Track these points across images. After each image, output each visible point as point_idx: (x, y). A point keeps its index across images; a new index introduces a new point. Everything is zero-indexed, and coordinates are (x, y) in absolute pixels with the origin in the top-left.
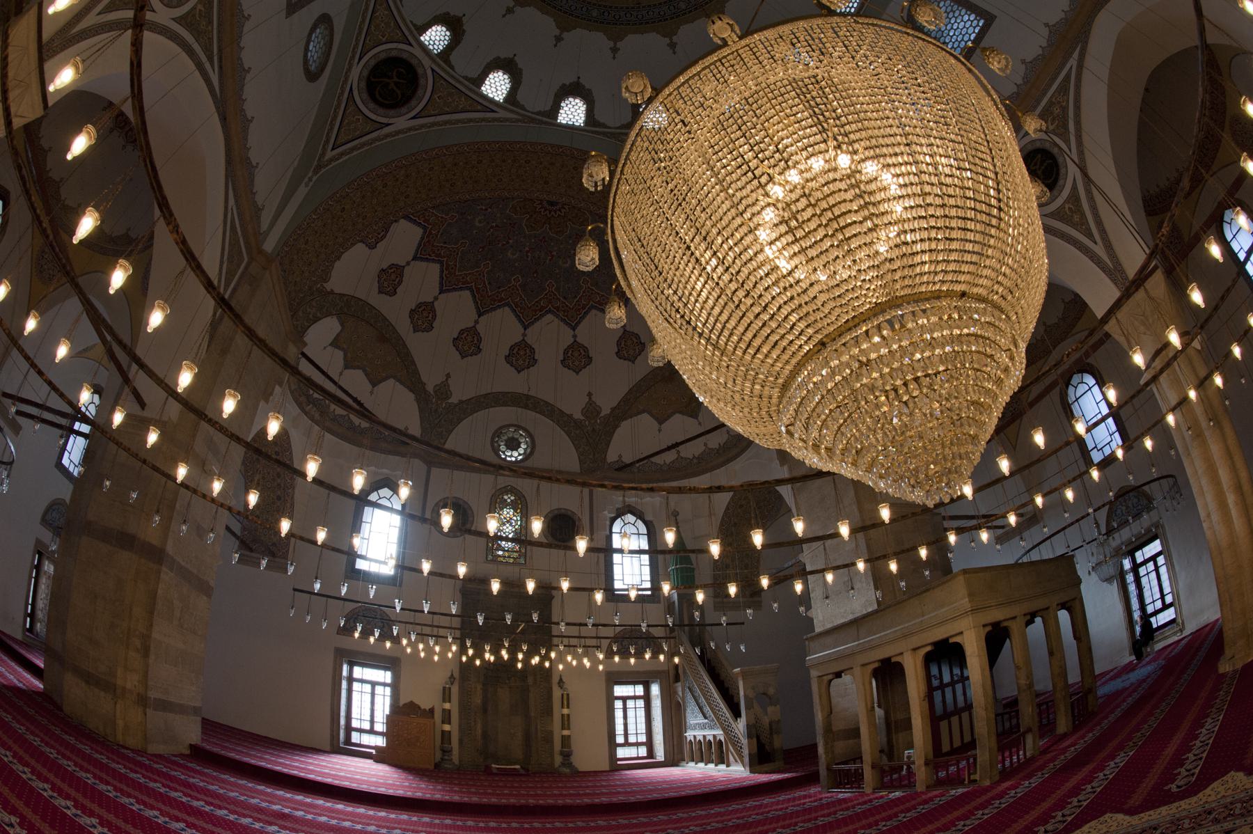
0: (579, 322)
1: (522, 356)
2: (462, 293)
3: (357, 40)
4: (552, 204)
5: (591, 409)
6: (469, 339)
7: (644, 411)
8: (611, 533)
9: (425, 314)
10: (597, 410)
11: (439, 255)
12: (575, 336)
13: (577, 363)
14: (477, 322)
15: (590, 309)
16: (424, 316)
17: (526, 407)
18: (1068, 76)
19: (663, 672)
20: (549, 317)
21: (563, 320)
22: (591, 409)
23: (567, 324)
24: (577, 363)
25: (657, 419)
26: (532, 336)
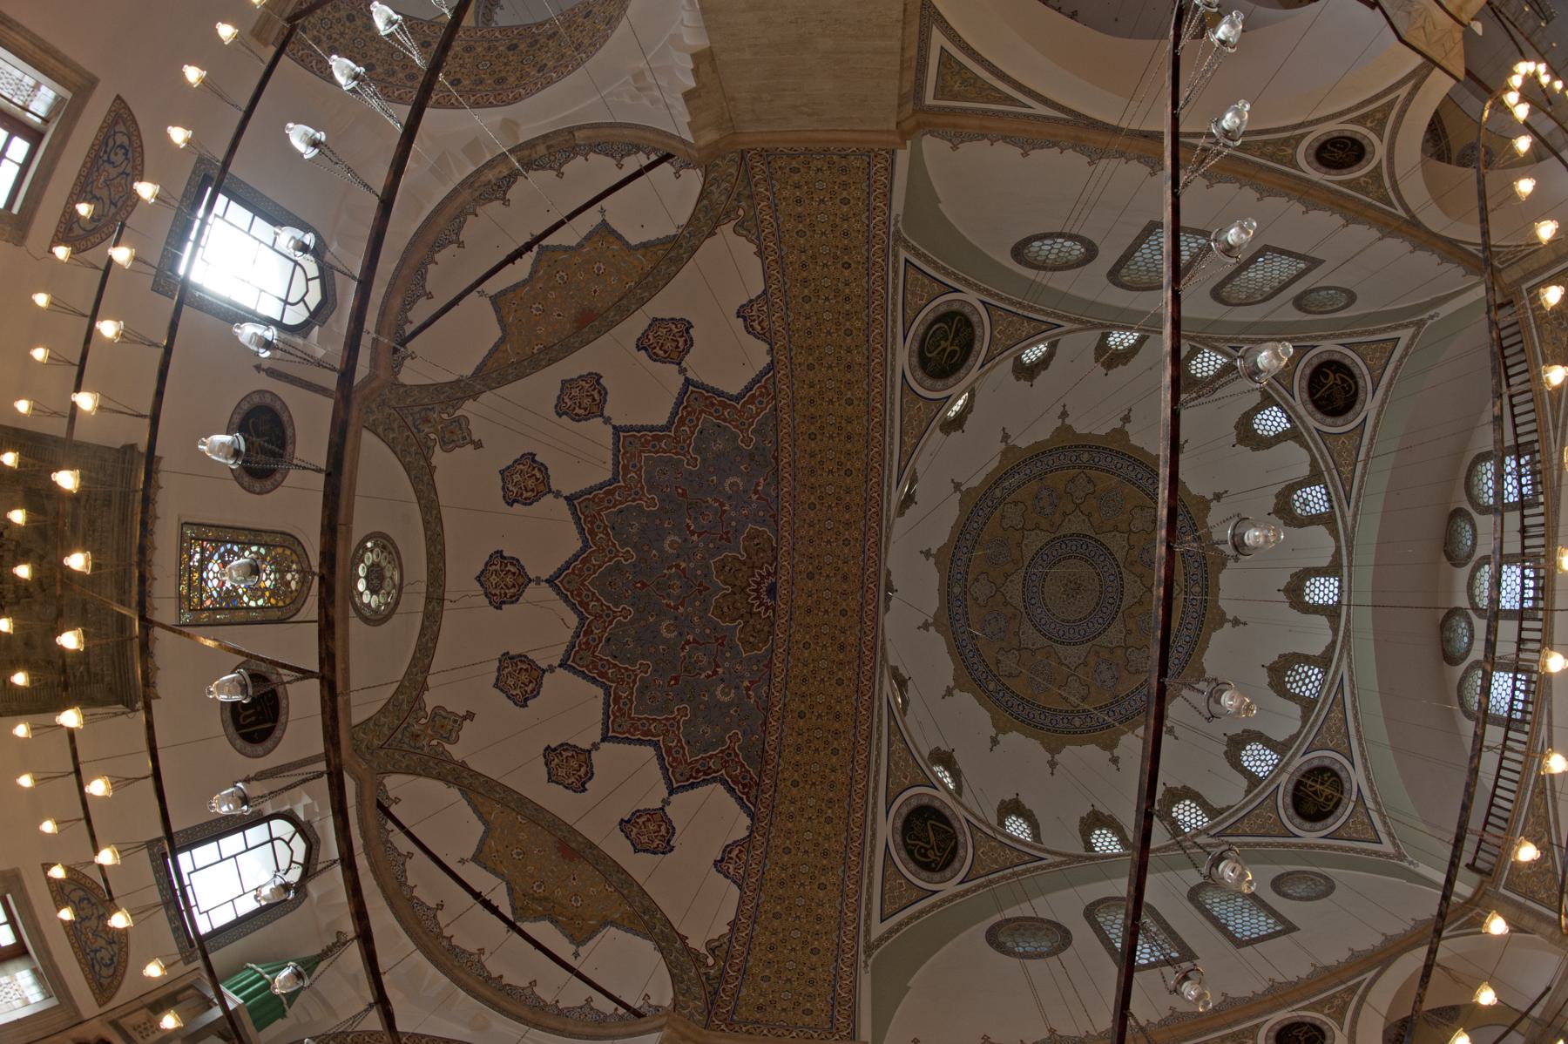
0: (575, 672)
1: (504, 580)
2: (610, 466)
3: (1001, 299)
4: (772, 591)
5: (448, 724)
6: (531, 483)
7: (485, 822)
8: (267, 819)
10: (451, 737)
12: (551, 669)
13: (511, 681)
14: (557, 494)
15: (602, 685)
16: (584, 400)
17: (429, 599)
18: (1359, 984)
19: (77, 1011)
20: (573, 620)
22: (448, 724)
24: (511, 681)
25: (479, 850)
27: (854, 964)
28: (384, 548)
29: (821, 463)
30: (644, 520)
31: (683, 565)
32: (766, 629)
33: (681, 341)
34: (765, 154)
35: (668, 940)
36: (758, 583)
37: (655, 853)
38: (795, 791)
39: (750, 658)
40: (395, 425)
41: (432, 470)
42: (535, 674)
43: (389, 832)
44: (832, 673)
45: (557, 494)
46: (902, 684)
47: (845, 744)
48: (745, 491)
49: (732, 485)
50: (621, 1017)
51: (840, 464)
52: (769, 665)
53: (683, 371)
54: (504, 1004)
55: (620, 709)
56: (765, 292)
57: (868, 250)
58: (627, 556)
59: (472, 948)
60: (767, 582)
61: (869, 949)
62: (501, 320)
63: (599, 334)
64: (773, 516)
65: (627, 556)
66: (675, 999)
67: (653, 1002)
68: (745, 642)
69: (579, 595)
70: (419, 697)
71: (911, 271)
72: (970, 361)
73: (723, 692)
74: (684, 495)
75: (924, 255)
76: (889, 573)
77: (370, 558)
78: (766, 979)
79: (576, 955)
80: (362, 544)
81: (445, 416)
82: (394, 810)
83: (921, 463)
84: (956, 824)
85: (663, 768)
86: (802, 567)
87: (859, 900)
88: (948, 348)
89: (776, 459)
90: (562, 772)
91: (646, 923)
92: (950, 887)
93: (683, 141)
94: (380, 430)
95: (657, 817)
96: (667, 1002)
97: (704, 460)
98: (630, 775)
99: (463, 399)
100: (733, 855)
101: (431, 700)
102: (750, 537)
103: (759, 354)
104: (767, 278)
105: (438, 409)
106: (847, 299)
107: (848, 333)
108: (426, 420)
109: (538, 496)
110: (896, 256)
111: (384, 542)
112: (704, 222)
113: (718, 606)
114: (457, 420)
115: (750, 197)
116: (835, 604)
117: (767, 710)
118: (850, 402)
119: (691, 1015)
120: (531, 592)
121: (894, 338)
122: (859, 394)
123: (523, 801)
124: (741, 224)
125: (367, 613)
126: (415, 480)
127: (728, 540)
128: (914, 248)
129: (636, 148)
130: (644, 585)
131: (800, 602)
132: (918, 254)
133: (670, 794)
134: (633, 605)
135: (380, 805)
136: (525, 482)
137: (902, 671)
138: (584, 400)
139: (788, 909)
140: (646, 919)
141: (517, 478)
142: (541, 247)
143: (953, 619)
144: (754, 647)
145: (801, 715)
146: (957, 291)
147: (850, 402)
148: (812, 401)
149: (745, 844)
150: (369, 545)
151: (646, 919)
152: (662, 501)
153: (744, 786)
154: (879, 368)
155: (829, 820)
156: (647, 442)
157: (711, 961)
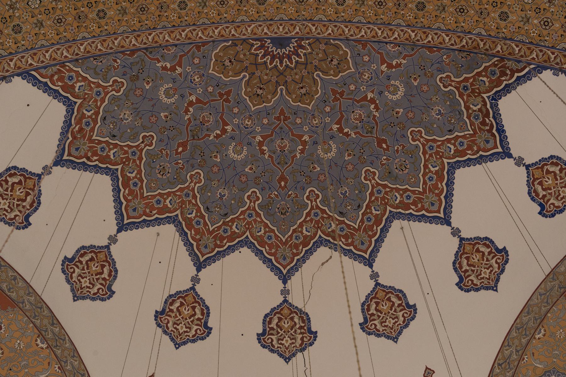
4: (281, 42)
12: (375, 276)
13: (390, 322)
14: (195, 280)
15: (389, 221)
16: (92, 271)
20: (323, 252)
21: (347, 253)
23: (356, 257)
30: (215, 183)
32: (322, 46)
36: (273, 58)
39: (356, 64)
45: (195, 280)
48: (174, 81)
49: (168, 95)
52: (364, 43)
55: (415, 203)
58: (253, 198)
60: (272, 49)
65: (253, 198)
68: (338, 69)
69: (296, 246)
73: (394, 93)
74: (184, 145)
89: (133, 52)
97: (145, 129)
102: (224, 70)
109: (199, 301)
113: (300, 98)
117: (414, 45)
120: (296, 300)
123: (518, 326)
127: (228, 93)
130: (282, 178)
134: (304, 189)
138: (92, 271)
141: (182, 328)
144: (343, 59)
148: (59, 21)
153: (503, 74)
156: (131, 192)
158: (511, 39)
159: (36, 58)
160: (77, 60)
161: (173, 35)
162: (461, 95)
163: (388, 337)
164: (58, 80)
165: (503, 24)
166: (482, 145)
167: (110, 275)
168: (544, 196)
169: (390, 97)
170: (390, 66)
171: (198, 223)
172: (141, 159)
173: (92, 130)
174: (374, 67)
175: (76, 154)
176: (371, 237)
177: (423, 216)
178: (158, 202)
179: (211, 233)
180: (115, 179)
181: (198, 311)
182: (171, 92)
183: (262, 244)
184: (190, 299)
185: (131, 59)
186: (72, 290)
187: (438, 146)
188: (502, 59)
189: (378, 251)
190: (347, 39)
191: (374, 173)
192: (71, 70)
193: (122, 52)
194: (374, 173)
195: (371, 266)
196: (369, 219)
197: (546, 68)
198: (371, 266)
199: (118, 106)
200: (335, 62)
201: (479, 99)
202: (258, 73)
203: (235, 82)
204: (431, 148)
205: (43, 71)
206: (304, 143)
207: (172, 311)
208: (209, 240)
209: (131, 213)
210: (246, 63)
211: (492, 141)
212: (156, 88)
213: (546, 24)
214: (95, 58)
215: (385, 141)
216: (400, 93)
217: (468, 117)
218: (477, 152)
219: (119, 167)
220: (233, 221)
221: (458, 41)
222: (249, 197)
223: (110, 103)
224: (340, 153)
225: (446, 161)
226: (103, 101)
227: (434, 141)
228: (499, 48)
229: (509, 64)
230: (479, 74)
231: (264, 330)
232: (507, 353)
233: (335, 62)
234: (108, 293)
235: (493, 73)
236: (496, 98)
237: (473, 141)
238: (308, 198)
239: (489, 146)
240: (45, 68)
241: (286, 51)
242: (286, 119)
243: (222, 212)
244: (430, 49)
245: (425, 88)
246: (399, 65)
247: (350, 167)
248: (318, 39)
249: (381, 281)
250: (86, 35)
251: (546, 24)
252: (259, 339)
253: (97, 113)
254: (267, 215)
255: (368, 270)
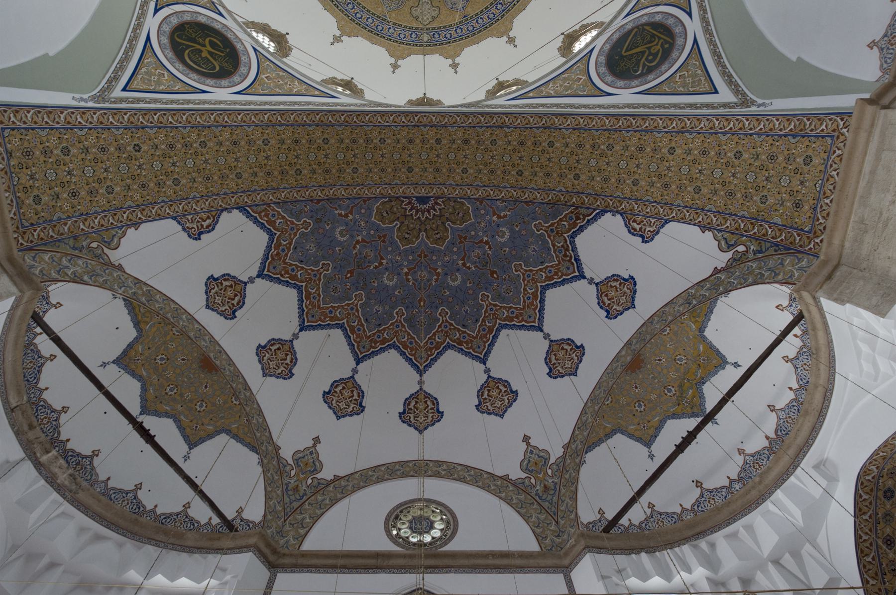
4: (423, 200)
5: (535, 460)
6: (347, 394)
9: (280, 355)
10: (544, 456)
11: (293, 277)
12: (487, 371)
13: (498, 404)
14: (355, 371)
20: (450, 353)
22: (535, 460)
25: (639, 440)
26: (433, 381)
27: (758, 117)
28: (397, 517)
29: (319, 164)
30: (373, 302)
31: (406, 270)
32: (452, 204)
33: (225, 283)
34: (22, 229)
35: (718, 284)
37: (635, 292)
38: (583, 177)
39: (475, 216)
40: (299, 517)
41: (337, 478)
42: (492, 384)
43: (631, 524)
44: (486, 150)
45: (355, 371)
46: (501, 86)
47: (545, 136)
50: (805, 332)
51: (319, 148)
52: (480, 200)
53: (251, 280)
54: (800, 440)
55: (517, 317)
56: (174, 218)
57: (118, 128)
59: (740, 460)
60: (417, 205)
61: (745, 102)
62: (210, 436)
63: (222, 351)
64: (365, 201)
66: (781, 283)
67: (785, 303)
68: (463, 220)
70: (514, 483)
71: (134, 85)
72: (217, 26)
74: (351, 272)
75: (116, 71)
76: (410, 102)
77: (405, 532)
78: (764, 199)
79: (736, 365)
80: (394, 539)
81: (293, 473)
82: (610, 516)
83: (316, 73)
84: (629, 27)
85: (563, 282)
86: (404, 177)
87: (689, 117)
88: (206, 48)
89: (319, 201)
90: (568, 364)
91: (700, 303)
92: (693, 26)
93: (14, 308)
94: (302, 532)
95: (604, 288)
96: (786, 290)
97: (324, 258)
98: (569, 309)
99: (279, 458)
100: (638, 227)
101: (516, 473)
103: (233, 222)
104: (160, 217)
105: (286, 480)
106: (171, 146)
107: (203, 145)
108: (296, 489)
110: (121, 100)
111: (393, 518)
112: (108, 276)
113: (436, 241)
114: (296, 461)
115: (75, 238)
116: (431, 148)
117: (516, 201)
118: (266, 142)
119: (801, 269)
121: (205, 102)
122: (258, 134)
124: (108, 244)
125: (449, 533)
126: (345, 493)
127: (385, 236)
128: (109, 81)
129: (30, 348)
131: (431, 177)
132: (115, 78)
133: (584, 277)
134: (437, 308)
135: (607, 530)
136: (345, 398)
137: (490, 86)
139: (691, 180)
140: (699, 301)
141: (342, 405)
142: (144, 410)
143: (447, 39)
144: (466, 213)
145: (520, 173)
146: (148, 38)
147: (266, 142)
149: (628, 218)
150: (395, 532)
151: (699, 301)
152: (357, 289)
153: (578, 218)
154: (233, 116)
155: (610, 147)
157: (741, 248)
158: (582, 193)
159: (250, 198)
160: (279, 203)
161: (347, 191)
162: (549, 237)
163: (496, 415)
164: (265, 216)
165: (576, 182)
166: (564, 271)
167: (291, 362)
168: (609, 304)
169: (499, 239)
170: (499, 217)
171: (359, 330)
172: (320, 280)
173: (286, 255)
174: (488, 218)
175: (273, 271)
176: (485, 342)
177: (523, 325)
178: (331, 312)
179: (368, 337)
180: (300, 292)
181: (355, 394)
182: (344, 233)
183: (406, 347)
184: (350, 384)
185: (317, 206)
186: (263, 369)
187: (534, 275)
188: (577, 208)
189: (490, 352)
190: (469, 198)
191: (488, 296)
192: (273, 210)
193: (311, 201)
194: (488, 296)
195: (485, 364)
196: (484, 330)
197: (607, 212)
198: (485, 364)
199: (306, 240)
200: (461, 215)
201: (562, 238)
202: (406, 222)
203: (391, 228)
204: (529, 276)
205: (254, 208)
206: (438, 274)
207: (336, 392)
208: (366, 342)
209: (310, 319)
210: (398, 215)
211: (571, 268)
212: (333, 229)
213: (606, 180)
214: (292, 202)
215: (495, 272)
216: (507, 237)
217: (555, 252)
218: (561, 276)
219: (304, 284)
220: (384, 330)
221: (546, 196)
222: (397, 313)
223: (300, 237)
224: (464, 282)
225: (539, 285)
226: (295, 235)
227: (531, 271)
228: (574, 200)
229: (582, 210)
230: (561, 220)
231: (404, 410)
232: (584, 419)
233: (461, 215)
234: (289, 375)
235: (571, 219)
236: (573, 237)
237: (558, 269)
238: (440, 314)
239: (569, 272)
240: (256, 206)
241: (427, 206)
242: (425, 256)
243: (377, 323)
244: (527, 203)
245: (524, 232)
246: (505, 216)
247: (471, 292)
248: (449, 198)
249: (492, 374)
250: (286, 185)
251: (606, 180)
252: (400, 417)
253: (290, 243)
254: (410, 327)
255: (482, 367)
